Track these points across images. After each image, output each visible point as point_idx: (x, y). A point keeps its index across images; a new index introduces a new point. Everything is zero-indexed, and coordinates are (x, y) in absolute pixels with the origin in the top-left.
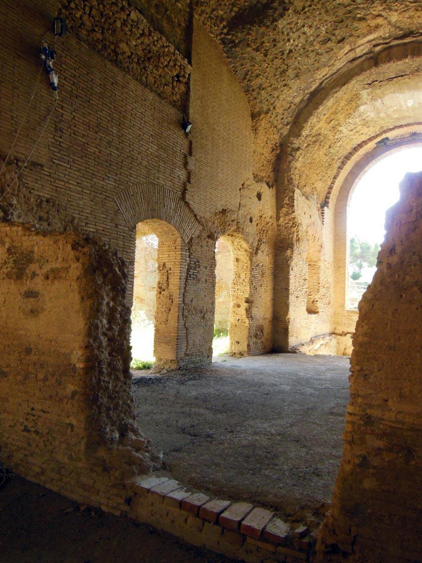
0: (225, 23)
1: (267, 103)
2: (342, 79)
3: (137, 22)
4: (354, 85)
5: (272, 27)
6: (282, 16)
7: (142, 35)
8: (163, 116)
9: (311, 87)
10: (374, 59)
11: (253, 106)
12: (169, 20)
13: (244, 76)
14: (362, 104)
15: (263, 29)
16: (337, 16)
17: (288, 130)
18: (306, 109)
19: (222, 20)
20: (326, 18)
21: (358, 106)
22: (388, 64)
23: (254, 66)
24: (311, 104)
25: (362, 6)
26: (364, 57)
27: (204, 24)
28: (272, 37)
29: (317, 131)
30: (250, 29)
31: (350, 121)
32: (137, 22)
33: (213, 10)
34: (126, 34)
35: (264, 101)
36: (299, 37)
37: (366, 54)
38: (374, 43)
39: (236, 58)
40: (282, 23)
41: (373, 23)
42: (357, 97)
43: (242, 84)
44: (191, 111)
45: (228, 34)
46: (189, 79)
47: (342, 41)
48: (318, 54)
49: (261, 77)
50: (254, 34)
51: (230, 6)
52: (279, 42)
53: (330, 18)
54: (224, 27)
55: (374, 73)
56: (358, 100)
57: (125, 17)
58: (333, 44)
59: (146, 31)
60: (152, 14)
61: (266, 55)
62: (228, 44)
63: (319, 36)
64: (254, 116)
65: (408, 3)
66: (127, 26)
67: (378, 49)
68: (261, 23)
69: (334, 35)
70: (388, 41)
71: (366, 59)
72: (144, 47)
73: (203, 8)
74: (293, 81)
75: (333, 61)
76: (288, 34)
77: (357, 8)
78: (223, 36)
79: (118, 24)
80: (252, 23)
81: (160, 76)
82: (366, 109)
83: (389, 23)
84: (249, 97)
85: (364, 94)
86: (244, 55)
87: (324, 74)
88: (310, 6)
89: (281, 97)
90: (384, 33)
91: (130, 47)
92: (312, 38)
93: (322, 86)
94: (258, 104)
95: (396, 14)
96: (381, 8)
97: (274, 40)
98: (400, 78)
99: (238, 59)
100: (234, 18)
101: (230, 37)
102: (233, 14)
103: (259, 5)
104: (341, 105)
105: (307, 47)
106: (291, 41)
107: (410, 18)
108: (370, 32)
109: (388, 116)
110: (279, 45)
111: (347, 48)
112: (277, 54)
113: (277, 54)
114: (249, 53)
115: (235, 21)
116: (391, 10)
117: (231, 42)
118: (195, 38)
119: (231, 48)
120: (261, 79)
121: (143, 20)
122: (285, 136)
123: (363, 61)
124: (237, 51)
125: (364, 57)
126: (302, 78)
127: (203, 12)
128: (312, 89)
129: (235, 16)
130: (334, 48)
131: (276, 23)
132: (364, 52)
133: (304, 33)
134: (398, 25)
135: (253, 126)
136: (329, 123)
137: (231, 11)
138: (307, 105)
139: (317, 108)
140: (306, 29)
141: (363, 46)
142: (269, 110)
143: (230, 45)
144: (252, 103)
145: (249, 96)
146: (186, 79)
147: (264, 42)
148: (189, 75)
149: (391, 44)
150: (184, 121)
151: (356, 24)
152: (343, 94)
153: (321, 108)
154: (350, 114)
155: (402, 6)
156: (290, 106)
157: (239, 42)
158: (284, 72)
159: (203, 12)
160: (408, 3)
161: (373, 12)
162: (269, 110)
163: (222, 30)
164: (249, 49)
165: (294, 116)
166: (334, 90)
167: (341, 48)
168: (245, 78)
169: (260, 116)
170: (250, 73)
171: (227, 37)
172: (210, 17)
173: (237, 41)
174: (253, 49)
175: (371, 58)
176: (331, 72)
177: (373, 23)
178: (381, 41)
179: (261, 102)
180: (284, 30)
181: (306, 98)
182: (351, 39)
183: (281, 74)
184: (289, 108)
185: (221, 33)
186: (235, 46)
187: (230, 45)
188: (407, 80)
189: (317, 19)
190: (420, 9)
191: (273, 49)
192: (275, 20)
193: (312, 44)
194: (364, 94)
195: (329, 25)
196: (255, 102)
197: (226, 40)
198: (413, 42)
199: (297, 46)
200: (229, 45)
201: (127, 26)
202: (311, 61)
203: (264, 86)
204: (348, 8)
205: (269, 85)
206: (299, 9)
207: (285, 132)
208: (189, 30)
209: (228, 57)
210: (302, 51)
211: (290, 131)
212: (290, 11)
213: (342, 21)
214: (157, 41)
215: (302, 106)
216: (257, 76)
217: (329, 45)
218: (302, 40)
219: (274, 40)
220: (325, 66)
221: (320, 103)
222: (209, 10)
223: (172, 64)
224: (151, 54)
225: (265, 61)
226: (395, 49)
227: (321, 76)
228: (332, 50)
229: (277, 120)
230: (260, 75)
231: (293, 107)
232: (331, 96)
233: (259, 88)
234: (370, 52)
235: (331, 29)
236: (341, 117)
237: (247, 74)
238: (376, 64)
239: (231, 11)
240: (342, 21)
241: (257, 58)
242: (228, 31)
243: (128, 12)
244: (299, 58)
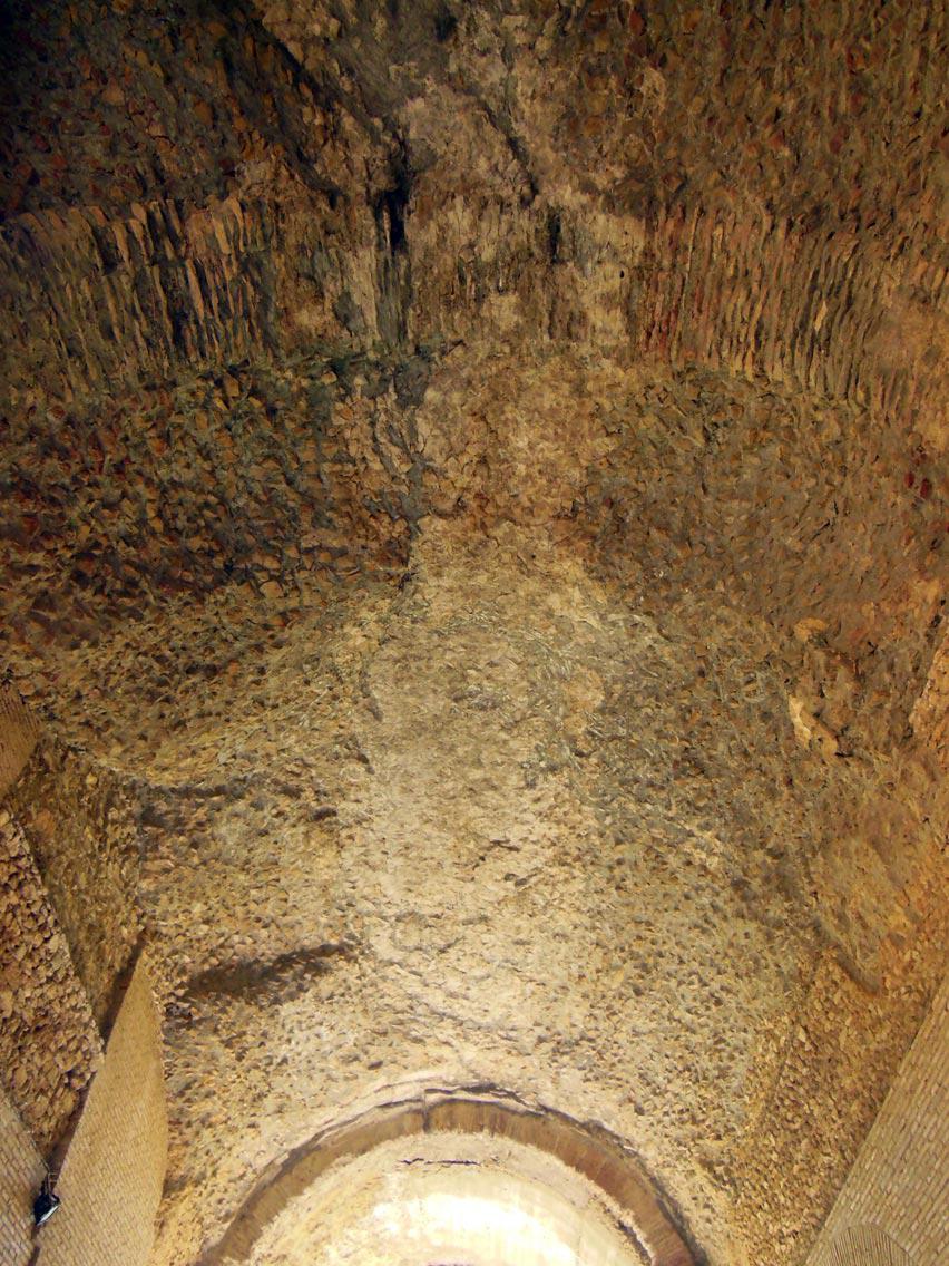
0: (185, 979)
1: (206, 1157)
2: (362, 1140)
3: (54, 956)
4: (382, 1156)
5: (270, 1011)
6: (292, 997)
7: (50, 980)
8: (9, 1173)
9: (297, 1139)
10: (426, 1117)
11: (175, 1162)
12: (100, 957)
13: (181, 1087)
14: (383, 1200)
15: (253, 1009)
16: (379, 1023)
17: (222, 1234)
18: (276, 1185)
19: (183, 971)
20: (361, 1020)
21: (375, 1203)
22: (449, 1134)
23: (210, 1073)
24: (287, 1178)
25: (422, 1019)
26: (406, 1107)
27: (152, 972)
28: (264, 1027)
29: (283, 1247)
30: (229, 1003)
31: (351, 1233)
32: (54, 956)
33: (175, 952)
34: (23, 973)
35: (200, 1154)
36: (308, 1039)
37: (410, 1101)
38: (428, 1085)
39: (182, 1048)
40: (287, 1009)
41: (434, 1052)
42: (378, 1181)
43: (170, 1104)
44: (67, 1164)
45: (183, 999)
46: (88, 1084)
47: (376, 1066)
48: (330, 1078)
49: (215, 1098)
50: (233, 1013)
51: (207, 954)
52: (272, 1040)
53: (368, 1023)
54: (181, 985)
55: (420, 1143)
56: (380, 1190)
57: (38, 943)
58: (361, 1068)
59: (60, 977)
60: (79, 942)
61: (240, 1058)
62: (176, 1017)
63: (340, 1046)
64: (170, 1187)
65: (497, 1038)
66: (33, 960)
67: (432, 1098)
68: (251, 998)
69: (366, 1053)
70: (450, 1088)
71: (411, 1111)
72: (42, 1004)
73: (160, 944)
74: (269, 1118)
75: (350, 1099)
76: (291, 1031)
77: (414, 1021)
78: (172, 999)
79: (21, 954)
80: (236, 994)
81: (41, 1070)
82: (387, 1214)
83: (461, 1060)
84: (174, 1138)
85: (394, 1178)
86: (199, 1047)
87: (328, 1118)
88: (343, 995)
89: (235, 1152)
90: (448, 1074)
91: (17, 1001)
92: (327, 1048)
93: (319, 1142)
94: (186, 1159)
95: (475, 1049)
96: (452, 1032)
97: (264, 1035)
98: (462, 1166)
99: (183, 1052)
100: (205, 975)
101: (186, 1005)
102: (207, 967)
103: (256, 966)
104: (346, 1193)
105: (315, 1061)
106: (293, 1042)
107: (496, 1062)
108: (425, 1066)
109: (424, 1238)
110: (269, 1045)
111: (382, 1081)
112: (260, 1061)
113: (260, 1061)
114: (210, 1045)
115: (205, 981)
116: (466, 1039)
117: (182, 1016)
118: (128, 997)
119: (180, 1026)
120: (214, 1103)
121: (65, 954)
122: (211, 1249)
123: (402, 1115)
124: (188, 1036)
125: (406, 1107)
126: (287, 1116)
127: (157, 951)
128: (296, 1145)
129: (208, 972)
130: (360, 1075)
131: (278, 1007)
132: (408, 1096)
133: (318, 1036)
134: (473, 1067)
135: (159, 1214)
136: (312, 1232)
137: (205, 961)
138: (278, 1178)
139: (299, 1192)
140: (323, 1030)
141: (409, 1084)
142: (203, 1176)
143: (179, 1021)
144: (175, 1153)
145: (176, 1135)
146: (83, 1084)
147: (244, 1033)
148: (93, 1074)
149: (455, 1096)
150: (43, 1189)
151: (406, 1045)
152: (355, 1170)
153: (308, 1192)
154: (356, 1217)
155: (488, 1039)
156: (244, 1175)
157: (200, 1022)
158: (261, 1096)
159: (157, 951)
160: (497, 1038)
161: (440, 1036)
162: (203, 1176)
163: (176, 988)
164: (214, 1039)
165: (244, 1200)
166: (342, 1159)
167: (372, 1079)
168: (181, 1094)
169: (182, 1189)
170: (197, 1085)
171: (179, 1003)
172: (164, 962)
173: (196, 1018)
174: (222, 1042)
175: (418, 1112)
176: (343, 1118)
177: (434, 1052)
178: (440, 1087)
179: (195, 1155)
180: (287, 1021)
181: (280, 1161)
182: (393, 1067)
183: (254, 1100)
184: (241, 1177)
185: (172, 994)
186: (189, 1026)
187: (179, 1021)
188: (475, 1174)
189: (347, 1018)
190: (514, 1052)
191: (257, 1050)
192: (277, 1001)
193: (324, 1058)
194: (394, 1178)
195: (363, 1033)
196: (182, 1152)
197: (174, 1009)
198: (492, 1104)
199: (299, 1054)
200: (179, 1020)
201: (33, 960)
202: (314, 1087)
203: (213, 1119)
204: (400, 1016)
205: (224, 1119)
206: (324, 995)
207: (215, 1236)
208: (122, 979)
209: (166, 1042)
210: (304, 1065)
211: (228, 1236)
212: (309, 995)
213: (385, 1034)
214: (69, 995)
215: (268, 1177)
216: (208, 1095)
217: (355, 1067)
218: (311, 1046)
219: (264, 1035)
220: (335, 1103)
221: (304, 1182)
222: (167, 950)
223: (73, 1046)
224: (46, 1021)
225: (234, 1069)
226: (462, 1108)
227: (322, 1121)
228: (356, 1077)
229: (209, 1205)
230: (214, 1093)
231: (250, 1176)
232: (331, 1171)
233: (203, 1122)
234: (419, 1100)
235: (364, 1041)
236: (335, 1219)
237: (188, 1087)
238: (427, 1127)
239: (205, 961)
240: (385, 1034)
241: (222, 1059)
242: (186, 994)
243: (46, 936)
244: (295, 1078)
